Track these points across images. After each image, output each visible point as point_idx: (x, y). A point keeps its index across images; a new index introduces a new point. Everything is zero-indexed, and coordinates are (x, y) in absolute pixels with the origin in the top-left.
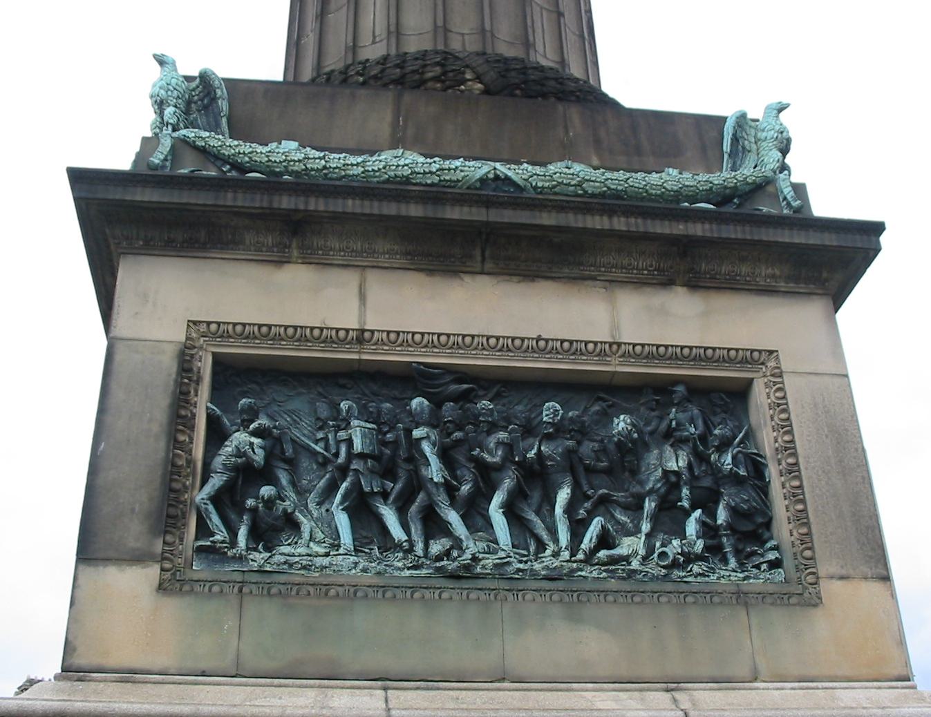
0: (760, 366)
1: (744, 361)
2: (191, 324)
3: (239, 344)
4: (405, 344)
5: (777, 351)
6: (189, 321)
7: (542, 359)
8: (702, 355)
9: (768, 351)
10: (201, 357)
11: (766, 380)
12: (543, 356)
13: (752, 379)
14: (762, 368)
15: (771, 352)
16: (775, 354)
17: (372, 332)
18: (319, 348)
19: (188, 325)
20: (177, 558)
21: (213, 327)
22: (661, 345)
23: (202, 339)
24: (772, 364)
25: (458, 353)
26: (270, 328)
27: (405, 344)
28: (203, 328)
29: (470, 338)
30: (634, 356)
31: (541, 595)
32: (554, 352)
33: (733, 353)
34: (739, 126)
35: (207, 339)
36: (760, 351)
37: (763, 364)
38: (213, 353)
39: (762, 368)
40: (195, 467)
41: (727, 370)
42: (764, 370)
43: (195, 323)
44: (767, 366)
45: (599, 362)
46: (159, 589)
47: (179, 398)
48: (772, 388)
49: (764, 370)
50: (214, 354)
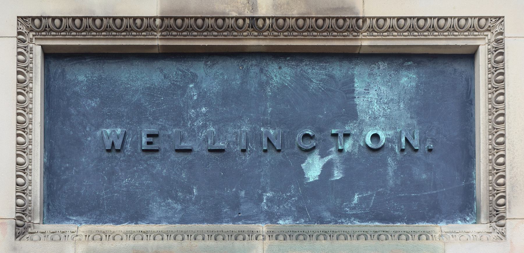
0: (486, 33)
1: (392, 28)
2: (20, 20)
3: (380, 37)
4: (271, 29)
5: (503, 17)
6: (18, 17)
7: (79, 37)
9: (495, 18)
10: (31, 48)
12: (442, 34)
13: (478, 46)
14: (487, 35)
15: (500, 18)
17: (264, 19)
18: (403, 37)
19: (18, 20)
22: (179, 18)
26: (41, 21)
27: (271, 29)
33: (422, 22)
34: (23, 212)
36: (487, 18)
37: (490, 30)
38: (42, 46)
39: (487, 35)
41: (246, 39)
42: (489, 37)
43: (22, 18)
50: (43, 47)
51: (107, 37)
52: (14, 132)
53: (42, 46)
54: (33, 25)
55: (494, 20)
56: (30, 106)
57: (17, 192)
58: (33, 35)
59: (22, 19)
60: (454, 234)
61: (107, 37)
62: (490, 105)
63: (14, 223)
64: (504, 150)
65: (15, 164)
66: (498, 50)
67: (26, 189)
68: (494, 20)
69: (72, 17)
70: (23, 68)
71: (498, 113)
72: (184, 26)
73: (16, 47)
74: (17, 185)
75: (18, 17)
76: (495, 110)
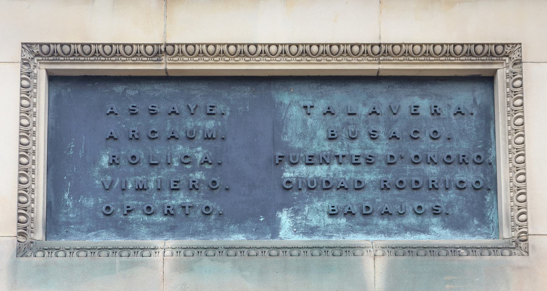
0: (504, 58)
2: (25, 46)
4: (448, 54)
5: (520, 44)
6: (22, 44)
8: (452, 51)
9: (513, 44)
11: (508, 71)
13: (495, 71)
14: (505, 60)
16: (518, 46)
19: (23, 47)
20: (30, 194)
21: (45, 48)
23: (36, 59)
24: (515, 56)
25: (79, 60)
28: (36, 50)
29: (296, 47)
30: (63, 55)
31: (430, 251)
32: (118, 54)
35: (40, 58)
37: (508, 56)
38: (46, 69)
39: (505, 60)
40: (508, 225)
42: (507, 61)
44: (510, 58)
45: (158, 62)
46: (124, 229)
47: (524, 150)
48: (512, 78)
49: (507, 61)
51: (465, 61)
52: (16, 173)
53: (46, 69)
54: (36, 51)
55: (511, 46)
56: (35, 109)
57: (19, 170)
58: (38, 60)
59: (27, 46)
60: (474, 250)
61: (465, 61)
62: (508, 89)
63: (16, 241)
64: (527, 228)
65: (16, 221)
66: (516, 76)
67: (29, 149)
68: (511, 46)
69: (329, 44)
70: (27, 91)
71: (517, 115)
72: (113, 52)
73: (19, 111)
74: (19, 222)
75: (22, 44)
76: (515, 169)
